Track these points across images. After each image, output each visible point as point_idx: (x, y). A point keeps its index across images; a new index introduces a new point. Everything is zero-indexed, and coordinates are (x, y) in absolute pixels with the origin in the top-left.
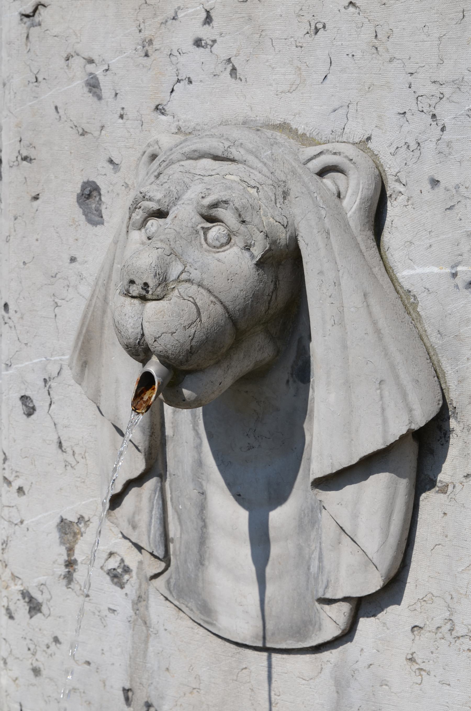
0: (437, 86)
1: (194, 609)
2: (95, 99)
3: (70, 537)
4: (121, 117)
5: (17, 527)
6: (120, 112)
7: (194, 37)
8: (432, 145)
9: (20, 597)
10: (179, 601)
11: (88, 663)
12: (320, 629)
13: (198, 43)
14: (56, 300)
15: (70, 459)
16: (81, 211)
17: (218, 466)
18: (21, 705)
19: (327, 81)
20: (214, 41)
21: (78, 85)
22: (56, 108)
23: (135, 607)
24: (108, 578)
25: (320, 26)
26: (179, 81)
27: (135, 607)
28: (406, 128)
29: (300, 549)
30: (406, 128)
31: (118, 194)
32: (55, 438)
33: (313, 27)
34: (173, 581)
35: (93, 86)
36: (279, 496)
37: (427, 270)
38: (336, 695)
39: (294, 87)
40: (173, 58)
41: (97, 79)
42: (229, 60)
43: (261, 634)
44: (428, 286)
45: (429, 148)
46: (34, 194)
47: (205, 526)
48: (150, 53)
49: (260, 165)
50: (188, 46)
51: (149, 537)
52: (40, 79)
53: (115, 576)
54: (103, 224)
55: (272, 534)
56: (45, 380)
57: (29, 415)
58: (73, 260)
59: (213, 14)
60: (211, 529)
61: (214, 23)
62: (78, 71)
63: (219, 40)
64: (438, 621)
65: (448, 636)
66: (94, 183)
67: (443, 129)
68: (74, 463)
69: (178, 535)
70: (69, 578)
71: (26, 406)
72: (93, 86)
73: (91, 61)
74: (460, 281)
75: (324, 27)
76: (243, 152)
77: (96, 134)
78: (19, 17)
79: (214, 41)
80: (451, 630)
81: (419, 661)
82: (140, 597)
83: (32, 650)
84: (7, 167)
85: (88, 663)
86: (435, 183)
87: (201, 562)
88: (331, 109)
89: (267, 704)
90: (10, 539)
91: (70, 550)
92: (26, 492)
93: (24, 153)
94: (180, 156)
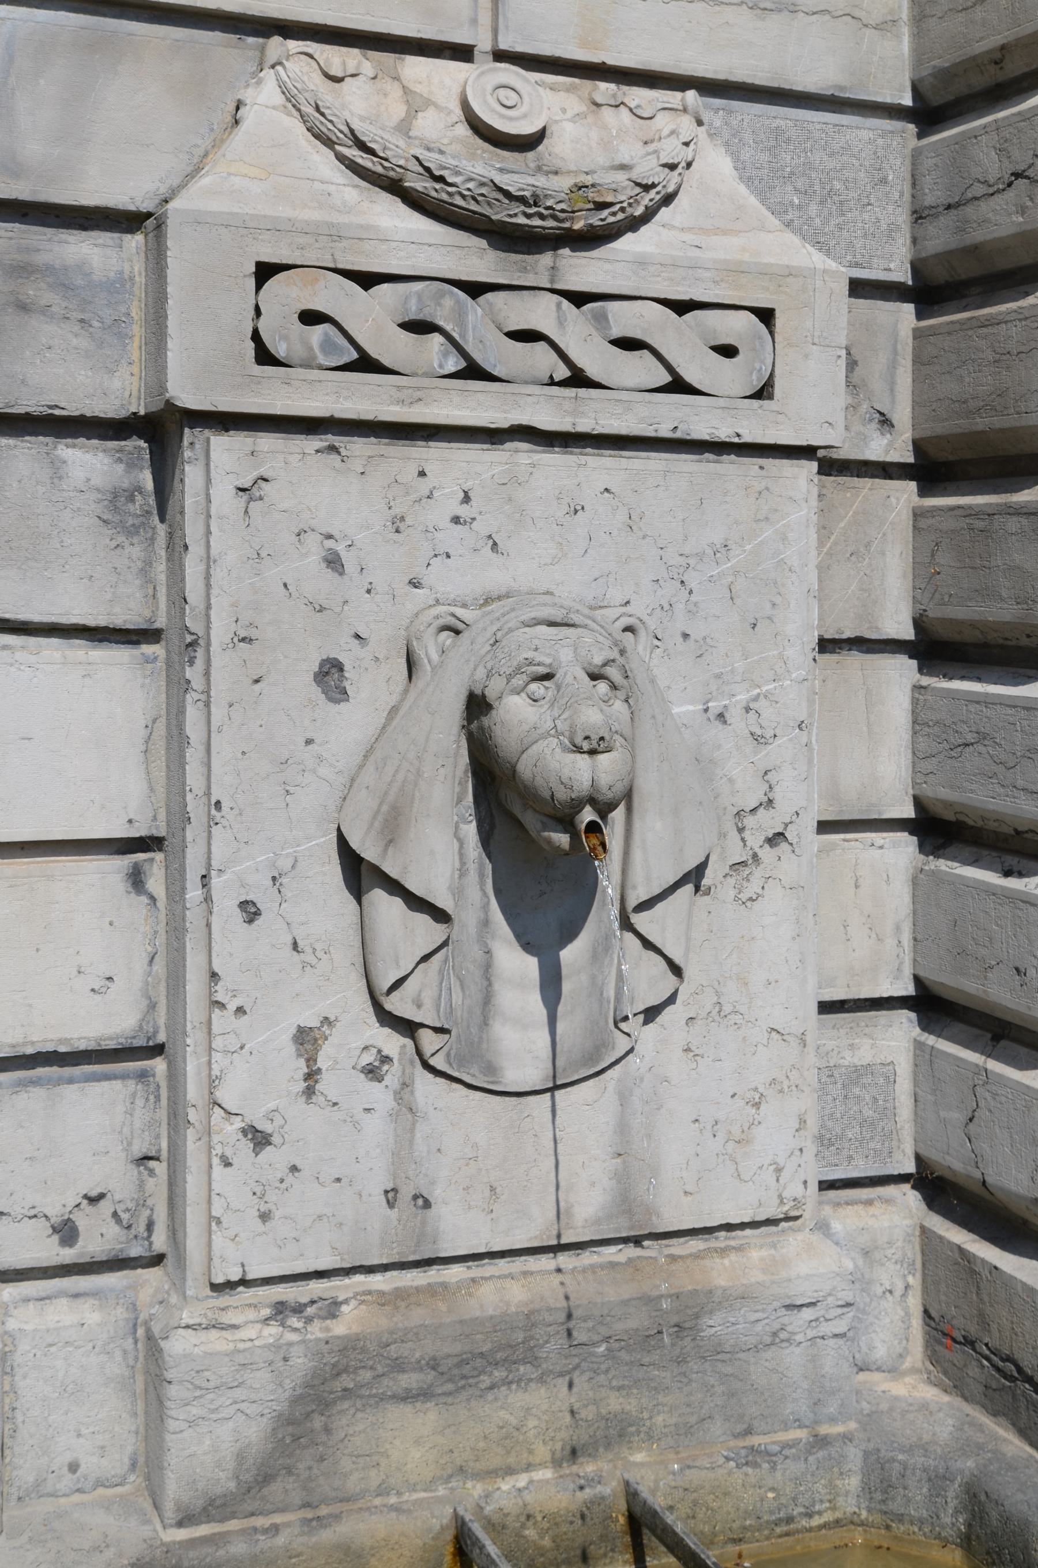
0: (683, 558)
1: (477, 1074)
2: (336, 575)
3: (308, 1047)
4: (369, 591)
5: (235, 1055)
6: (367, 586)
7: (452, 515)
8: (682, 606)
9: (240, 1136)
10: (459, 1071)
11: (338, 1180)
12: (613, 1048)
13: (456, 520)
14: (288, 788)
15: (310, 958)
16: (320, 689)
17: (507, 920)
18: (243, 1265)
19: (587, 555)
20: (474, 519)
21: (314, 561)
22: (285, 585)
23: (398, 1096)
24: (362, 1076)
25: (579, 508)
26: (436, 556)
27: (398, 1096)
28: (660, 593)
29: (593, 977)
30: (660, 593)
31: (367, 669)
32: (289, 940)
33: (572, 509)
34: (453, 1053)
35: (334, 562)
36: (569, 933)
37: (684, 709)
38: (620, 1108)
39: (556, 560)
40: (429, 535)
41: (338, 555)
42: (490, 537)
43: (552, 1074)
44: (685, 722)
45: (680, 608)
46: (255, 678)
47: (490, 985)
48: (402, 529)
49: (599, 628)
50: (445, 523)
51: (438, 1011)
52: (263, 554)
53: (371, 1071)
54: (348, 700)
55: (564, 971)
56: (274, 879)
57: (250, 921)
58: (309, 742)
59: (471, 494)
60: (496, 986)
61: (473, 503)
62: (314, 545)
63: (478, 518)
64: (708, 1007)
65: (717, 1018)
66: (335, 659)
67: (691, 592)
68: (314, 961)
69: (460, 1003)
70: (309, 1092)
71: (246, 912)
72: (334, 562)
73: (330, 537)
74: (711, 714)
75: (583, 508)
76: (582, 618)
77: (338, 609)
78: (234, 491)
79: (474, 519)
80: (719, 1012)
81: (693, 1048)
82: (404, 1084)
83: (258, 1194)
84: (220, 650)
85: (338, 1180)
86: (686, 636)
87: (485, 1023)
88: (593, 578)
89: (552, 1143)
90: (225, 1071)
91: (311, 1060)
92: (248, 1011)
93: (243, 634)
94: (519, 625)
